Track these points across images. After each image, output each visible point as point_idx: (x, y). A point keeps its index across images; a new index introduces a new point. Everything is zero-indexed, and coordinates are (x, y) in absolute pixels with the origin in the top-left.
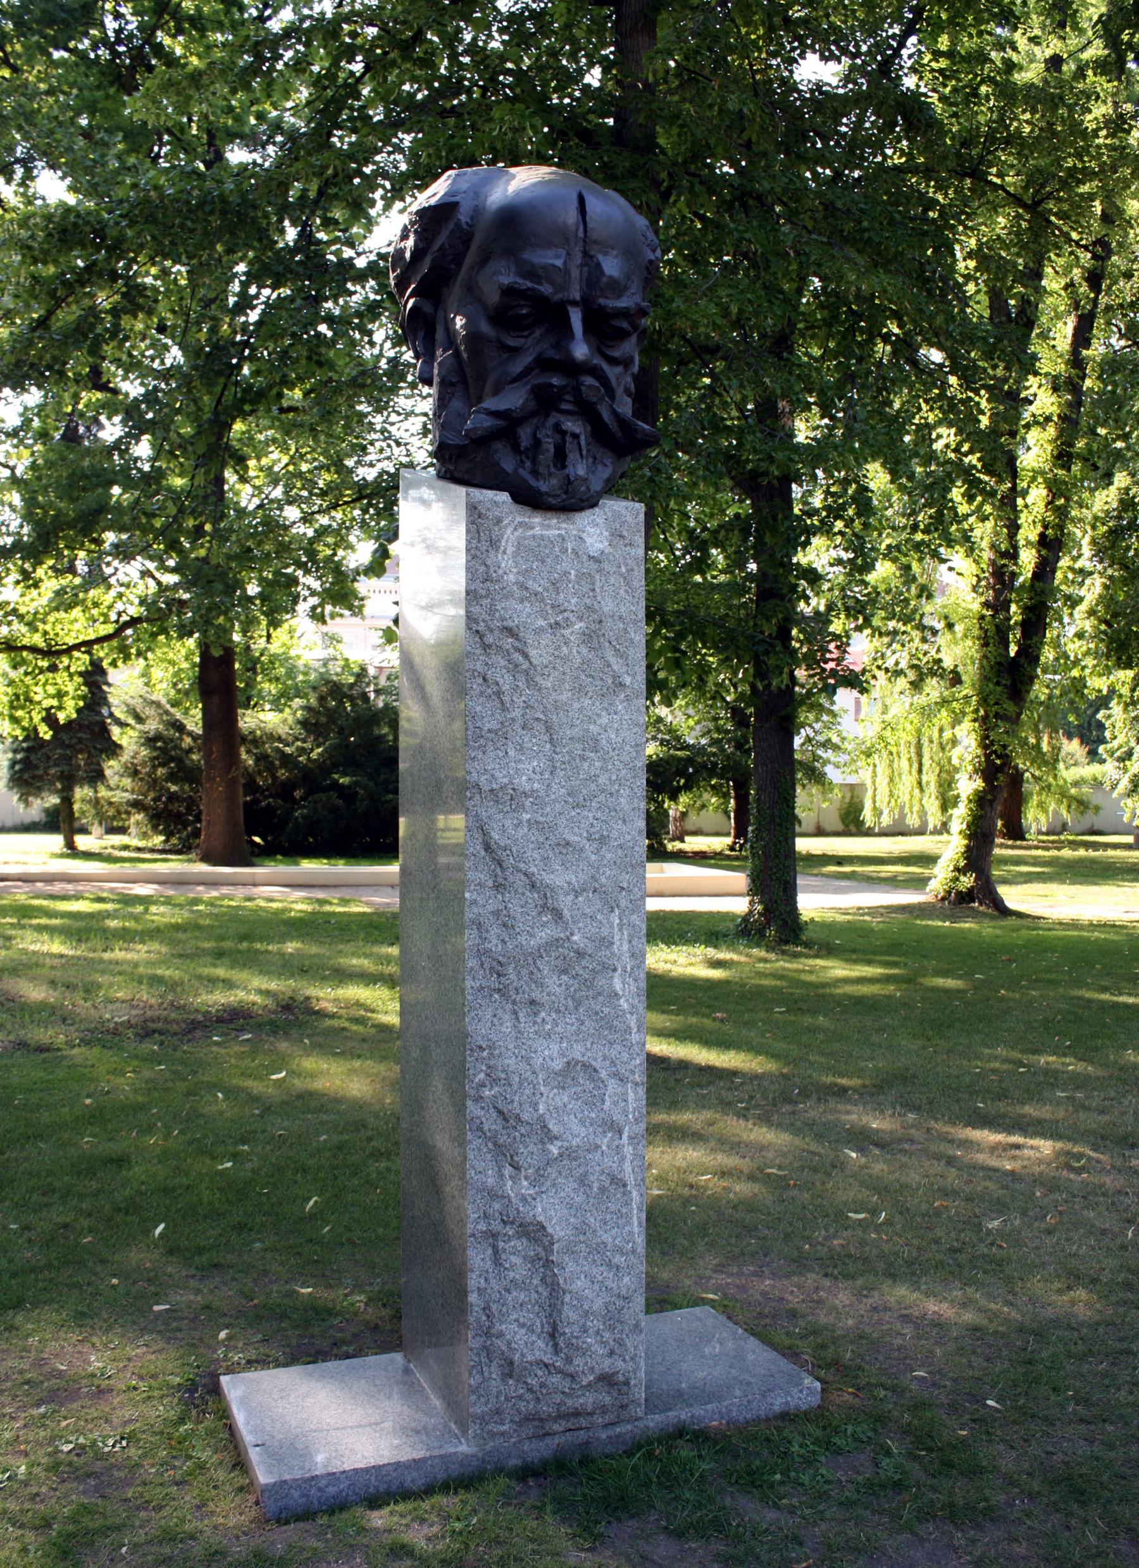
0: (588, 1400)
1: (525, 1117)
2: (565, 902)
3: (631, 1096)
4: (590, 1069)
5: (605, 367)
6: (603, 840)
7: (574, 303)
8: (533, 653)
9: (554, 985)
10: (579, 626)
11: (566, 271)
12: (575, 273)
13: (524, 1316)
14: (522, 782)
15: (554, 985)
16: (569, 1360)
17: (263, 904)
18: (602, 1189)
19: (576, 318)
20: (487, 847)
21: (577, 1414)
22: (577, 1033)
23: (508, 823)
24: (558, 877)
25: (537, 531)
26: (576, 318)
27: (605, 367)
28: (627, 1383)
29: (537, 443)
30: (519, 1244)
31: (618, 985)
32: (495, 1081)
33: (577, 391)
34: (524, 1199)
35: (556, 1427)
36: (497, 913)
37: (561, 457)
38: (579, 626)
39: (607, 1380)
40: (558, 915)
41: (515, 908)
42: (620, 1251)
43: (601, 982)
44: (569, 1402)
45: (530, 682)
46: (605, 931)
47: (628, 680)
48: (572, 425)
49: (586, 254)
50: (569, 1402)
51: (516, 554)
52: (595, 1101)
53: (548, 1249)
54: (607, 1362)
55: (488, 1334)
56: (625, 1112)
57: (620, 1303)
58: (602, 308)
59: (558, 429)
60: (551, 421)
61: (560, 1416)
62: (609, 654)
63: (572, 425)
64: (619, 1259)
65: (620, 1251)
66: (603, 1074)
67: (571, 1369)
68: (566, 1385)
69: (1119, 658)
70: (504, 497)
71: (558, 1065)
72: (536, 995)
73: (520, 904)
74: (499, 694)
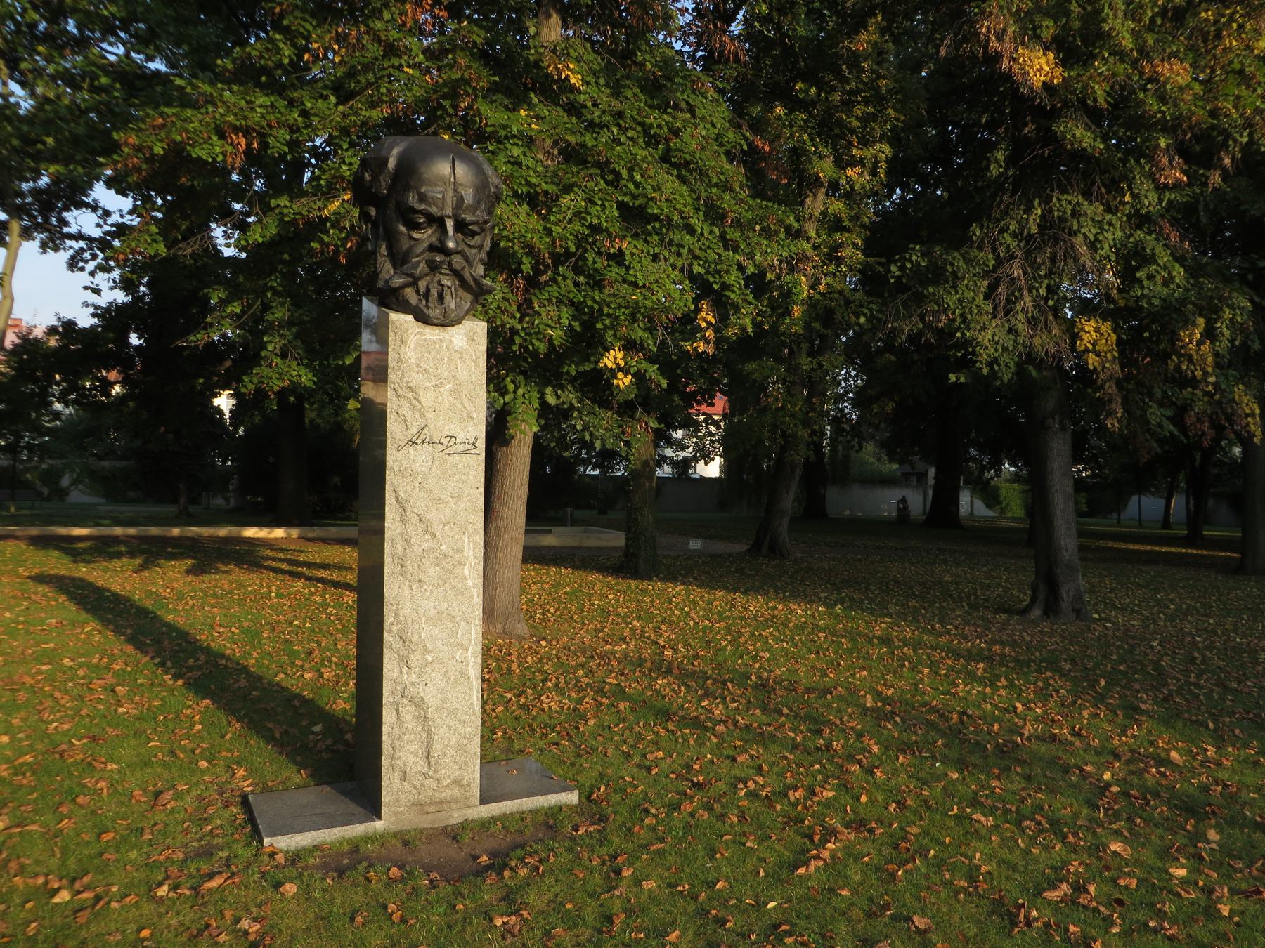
0: (447, 794)
1: (414, 640)
2: (437, 529)
3: (473, 631)
4: (452, 617)
5: (467, 250)
6: (459, 498)
7: (449, 217)
8: (423, 400)
9: (432, 572)
10: (449, 386)
11: (444, 199)
12: (449, 201)
13: (413, 747)
14: (416, 467)
15: (432, 572)
16: (436, 771)
17: (1098, 735)
18: (456, 680)
19: (450, 224)
20: (397, 500)
21: (441, 802)
22: (445, 597)
23: (408, 487)
24: (434, 515)
25: (427, 337)
26: (450, 224)
27: (467, 250)
28: (468, 785)
29: (428, 290)
30: (411, 708)
31: (466, 572)
32: (399, 622)
33: (450, 264)
34: (413, 684)
35: (430, 810)
36: (402, 534)
37: (441, 297)
38: (449, 386)
39: (457, 782)
40: (434, 536)
41: (411, 533)
42: (464, 713)
43: (457, 571)
44: (437, 795)
45: (422, 415)
46: (459, 544)
47: (475, 415)
48: (447, 282)
49: (455, 190)
50: (437, 795)
51: (416, 348)
52: (453, 633)
53: (426, 712)
54: (457, 773)
55: (393, 758)
56: (470, 640)
57: (465, 741)
58: (463, 220)
59: (439, 283)
60: (436, 279)
61: (432, 804)
62: (465, 400)
63: (447, 282)
64: (464, 717)
65: (464, 713)
66: (458, 619)
67: (437, 776)
68: (435, 785)
69: (1130, 94)
70: (410, 318)
71: (433, 613)
72: (422, 577)
73: (414, 529)
74: (405, 421)
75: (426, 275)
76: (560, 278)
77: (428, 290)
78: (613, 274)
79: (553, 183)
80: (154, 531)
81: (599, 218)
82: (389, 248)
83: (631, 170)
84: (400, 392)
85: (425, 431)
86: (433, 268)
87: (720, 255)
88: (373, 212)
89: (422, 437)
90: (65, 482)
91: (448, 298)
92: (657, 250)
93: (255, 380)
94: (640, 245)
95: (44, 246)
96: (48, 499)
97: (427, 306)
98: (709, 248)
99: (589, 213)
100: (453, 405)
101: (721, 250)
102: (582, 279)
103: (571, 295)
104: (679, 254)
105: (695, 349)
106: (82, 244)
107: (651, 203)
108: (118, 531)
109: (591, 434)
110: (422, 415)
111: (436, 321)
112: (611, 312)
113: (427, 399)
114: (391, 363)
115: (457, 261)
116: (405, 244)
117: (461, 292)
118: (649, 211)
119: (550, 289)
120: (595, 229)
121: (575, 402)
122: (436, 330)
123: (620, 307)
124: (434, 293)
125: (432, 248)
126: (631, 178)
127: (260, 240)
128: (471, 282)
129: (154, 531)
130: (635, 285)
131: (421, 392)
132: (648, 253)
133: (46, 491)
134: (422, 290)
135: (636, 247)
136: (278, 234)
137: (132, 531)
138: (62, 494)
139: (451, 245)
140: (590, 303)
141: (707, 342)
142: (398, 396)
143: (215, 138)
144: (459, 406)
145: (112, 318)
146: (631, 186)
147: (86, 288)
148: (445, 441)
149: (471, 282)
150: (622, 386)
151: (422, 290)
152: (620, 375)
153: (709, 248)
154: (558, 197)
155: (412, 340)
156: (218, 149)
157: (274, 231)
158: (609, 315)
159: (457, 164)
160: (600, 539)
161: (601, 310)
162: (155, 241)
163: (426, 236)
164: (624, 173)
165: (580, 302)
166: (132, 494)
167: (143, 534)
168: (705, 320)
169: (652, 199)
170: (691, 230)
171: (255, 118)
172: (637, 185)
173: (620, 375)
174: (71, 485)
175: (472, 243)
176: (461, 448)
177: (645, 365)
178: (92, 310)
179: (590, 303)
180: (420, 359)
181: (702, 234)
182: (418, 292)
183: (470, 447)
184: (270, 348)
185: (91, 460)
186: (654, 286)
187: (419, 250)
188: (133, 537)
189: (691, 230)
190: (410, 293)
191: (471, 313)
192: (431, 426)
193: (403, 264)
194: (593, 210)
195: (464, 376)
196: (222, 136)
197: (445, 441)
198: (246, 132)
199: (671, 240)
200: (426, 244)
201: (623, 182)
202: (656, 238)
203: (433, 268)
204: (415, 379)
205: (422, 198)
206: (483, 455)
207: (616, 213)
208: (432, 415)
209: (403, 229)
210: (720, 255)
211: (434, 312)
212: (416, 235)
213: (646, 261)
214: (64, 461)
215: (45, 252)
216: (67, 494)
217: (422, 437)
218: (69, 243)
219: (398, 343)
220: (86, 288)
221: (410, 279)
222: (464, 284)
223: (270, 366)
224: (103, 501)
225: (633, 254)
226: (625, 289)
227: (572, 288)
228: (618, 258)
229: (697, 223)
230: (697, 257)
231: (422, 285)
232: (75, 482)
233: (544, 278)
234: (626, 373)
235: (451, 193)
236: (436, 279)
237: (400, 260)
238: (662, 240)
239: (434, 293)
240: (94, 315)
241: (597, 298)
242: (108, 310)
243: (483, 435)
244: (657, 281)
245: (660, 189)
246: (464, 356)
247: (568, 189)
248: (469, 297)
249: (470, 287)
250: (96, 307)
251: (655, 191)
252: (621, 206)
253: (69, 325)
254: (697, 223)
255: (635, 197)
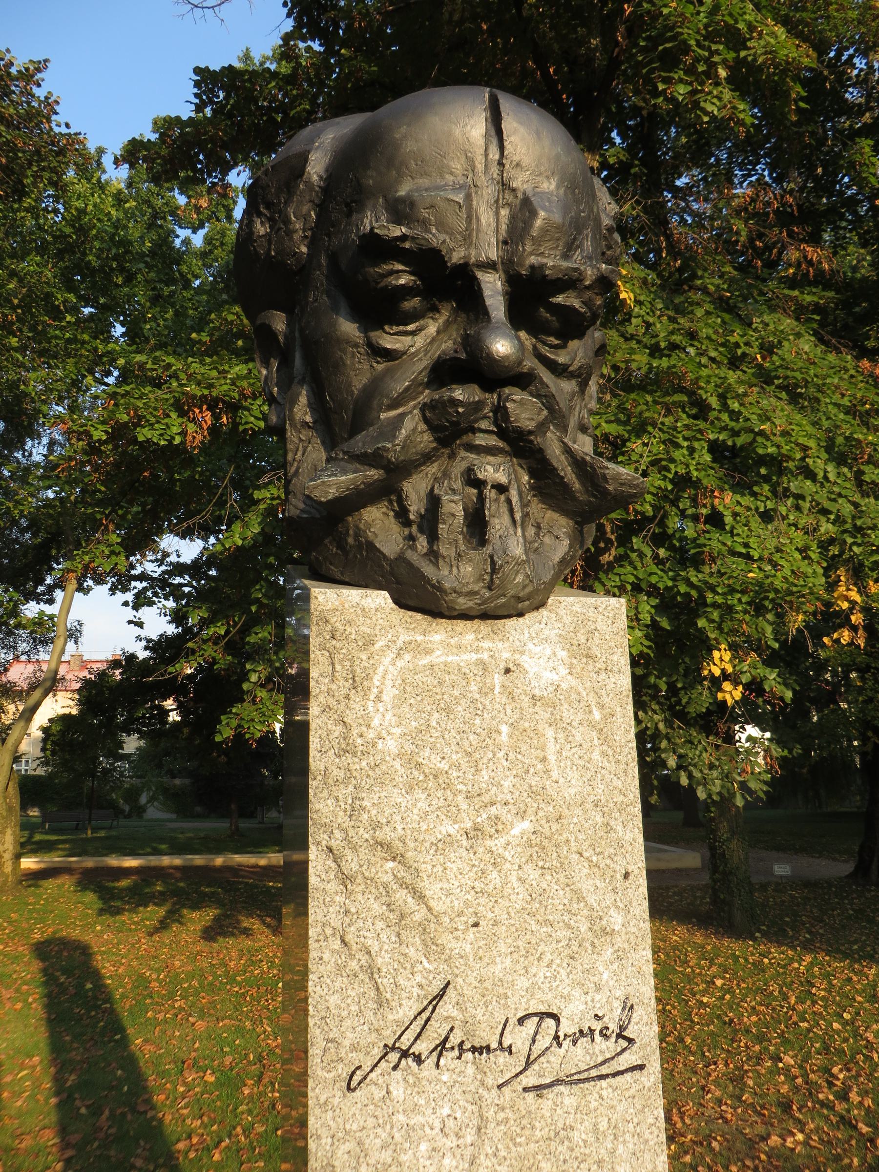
7: (490, 266)
8: (432, 889)
10: (525, 826)
12: (486, 217)
25: (438, 657)
26: (493, 287)
29: (434, 502)
33: (500, 411)
37: (477, 525)
38: (525, 826)
45: (431, 947)
47: (616, 920)
48: (493, 471)
51: (400, 700)
60: (458, 467)
63: (493, 471)
70: (381, 599)
74: (371, 971)
75: (427, 458)
76: (634, 556)
77: (434, 502)
78: (714, 544)
79: (618, 421)
80: (198, 860)
81: (687, 466)
82: (318, 404)
83: (722, 397)
84: (351, 864)
85: (446, 1008)
86: (450, 431)
87: (856, 505)
88: (279, 323)
89: (436, 1031)
90: (143, 800)
91: (498, 522)
92: (770, 505)
93: (234, 723)
94: (747, 500)
95: (113, 590)
96: (129, 816)
97: (433, 555)
98: (840, 495)
99: (672, 460)
100: (537, 896)
101: (857, 498)
102: (662, 552)
103: (654, 579)
104: (798, 508)
105: (837, 641)
106: (145, 584)
107: (759, 439)
108: (166, 861)
109: (690, 776)
110: (431, 947)
111: (463, 603)
112: (719, 599)
113: (448, 885)
114: (320, 758)
115: (523, 409)
116: (359, 372)
117: (536, 508)
118: (761, 451)
119: (621, 571)
120: (683, 482)
121: (661, 726)
122: (468, 633)
123: (732, 590)
124: (454, 509)
125: (444, 372)
126: (725, 407)
127: (240, 543)
128: (568, 473)
129: (198, 860)
130: (748, 557)
131: (425, 861)
132: (757, 509)
133: (127, 808)
134: (416, 506)
135: (739, 503)
136: (262, 532)
137: (177, 861)
138: (139, 811)
139: (502, 346)
140: (683, 588)
141: (854, 628)
142: (345, 879)
143: (174, 415)
144: (561, 897)
145: (165, 649)
146: (725, 417)
147: (130, 622)
148: (519, 1038)
149: (568, 473)
150: (730, 702)
151: (416, 506)
152: (727, 686)
153: (840, 495)
154: (624, 442)
155: (387, 672)
156: (175, 430)
157: (257, 529)
158: (715, 605)
159: (508, 124)
160: (659, 860)
161: (702, 597)
162: (113, 553)
163: (425, 339)
164: (714, 402)
165: (667, 588)
166: (198, 809)
167: (187, 864)
168: (847, 598)
169: (762, 433)
170: (810, 475)
171: (222, 388)
172: (735, 415)
173: (727, 686)
174: (148, 802)
175: (562, 358)
176: (579, 1056)
177: (762, 671)
178: (144, 643)
179: (683, 588)
180: (416, 737)
181: (826, 478)
182: (402, 515)
183: (609, 1047)
184: (254, 678)
185: (165, 779)
186: (776, 557)
187: (400, 385)
188: (176, 868)
189: (810, 475)
190: (379, 524)
191: (587, 575)
192: (465, 985)
193: (354, 431)
194: (677, 454)
195: (570, 784)
196: (182, 414)
197: (519, 1038)
198: (212, 404)
199: (787, 489)
200: (420, 367)
201: (713, 415)
202: (766, 487)
203: (450, 431)
204: (401, 809)
205: (401, 211)
206: (655, 1066)
207: (708, 458)
208: (465, 944)
209: (349, 328)
210: (856, 505)
211: (460, 573)
212: (389, 342)
213: (755, 522)
214: (144, 780)
215: (114, 594)
216: (145, 811)
217: (436, 1031)
218: (133, 584)
219: (342, 686)
220: (130, 622)
221: (374, 474)
222: (546, 482)
223: (254, 702)
224: (174, 816)
225: (735, 515)
226: (736, 565)
227: (654, 568)
228: (715, 519)
229: (819, 463)
230: (825, 512)
231: (415, 490)
232: (151, 800)
233: (606, 558)
234: (736, 683)
235: (488, 192)
236: (458, 467)
237: (342, 422)
238: (774, 492)
239: (454, 509)
240: (146, 648)
241: (694, 580)
242: (158, 643)
243: (645, 990)
244: (778, 550)
245: (768, 419)
246: (566, 713)
247: (640, 430)
248: (563, 524)
249: (565, 487)
250: (149, 641)
251: (763, 422)
252: (715, 448)
253: (131, 658)
254: (819, 463)
255: (735, 434)
